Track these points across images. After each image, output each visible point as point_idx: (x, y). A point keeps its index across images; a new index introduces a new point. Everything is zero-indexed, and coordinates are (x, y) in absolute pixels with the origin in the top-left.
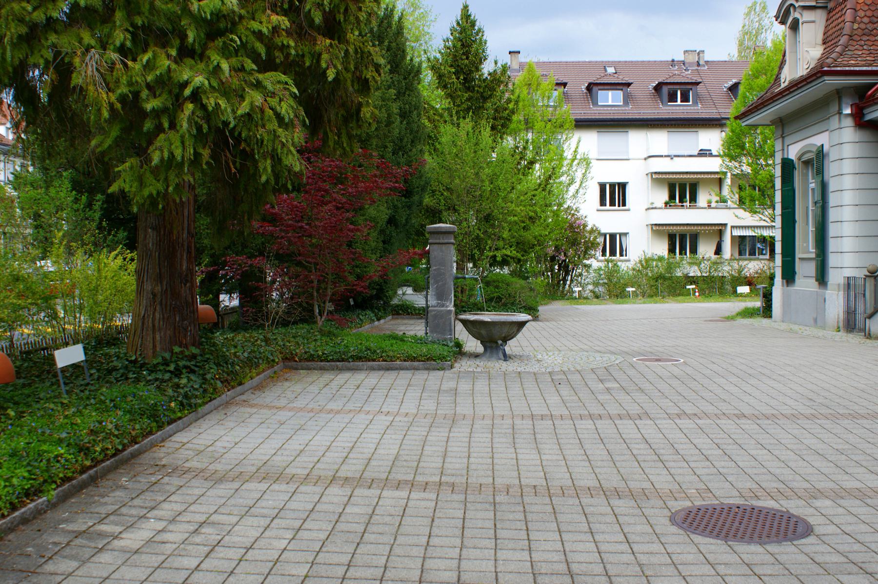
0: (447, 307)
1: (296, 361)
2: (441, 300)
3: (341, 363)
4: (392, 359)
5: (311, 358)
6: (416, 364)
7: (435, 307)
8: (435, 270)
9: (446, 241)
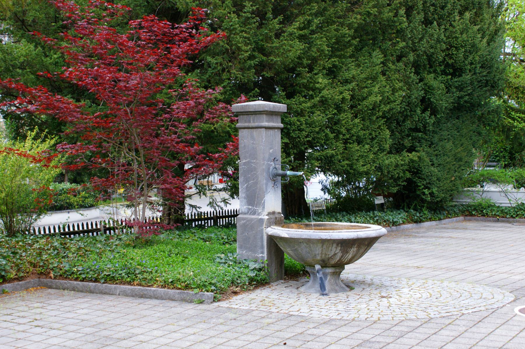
0: (259, 214)
1: (51, 277)
2: (252, 205)
3: (94, 284)
4: (148, 283)
5: (66, 275)
6: (171, 292)
7: (245, 214)
8: (245, 164)
9: (256, 124)
